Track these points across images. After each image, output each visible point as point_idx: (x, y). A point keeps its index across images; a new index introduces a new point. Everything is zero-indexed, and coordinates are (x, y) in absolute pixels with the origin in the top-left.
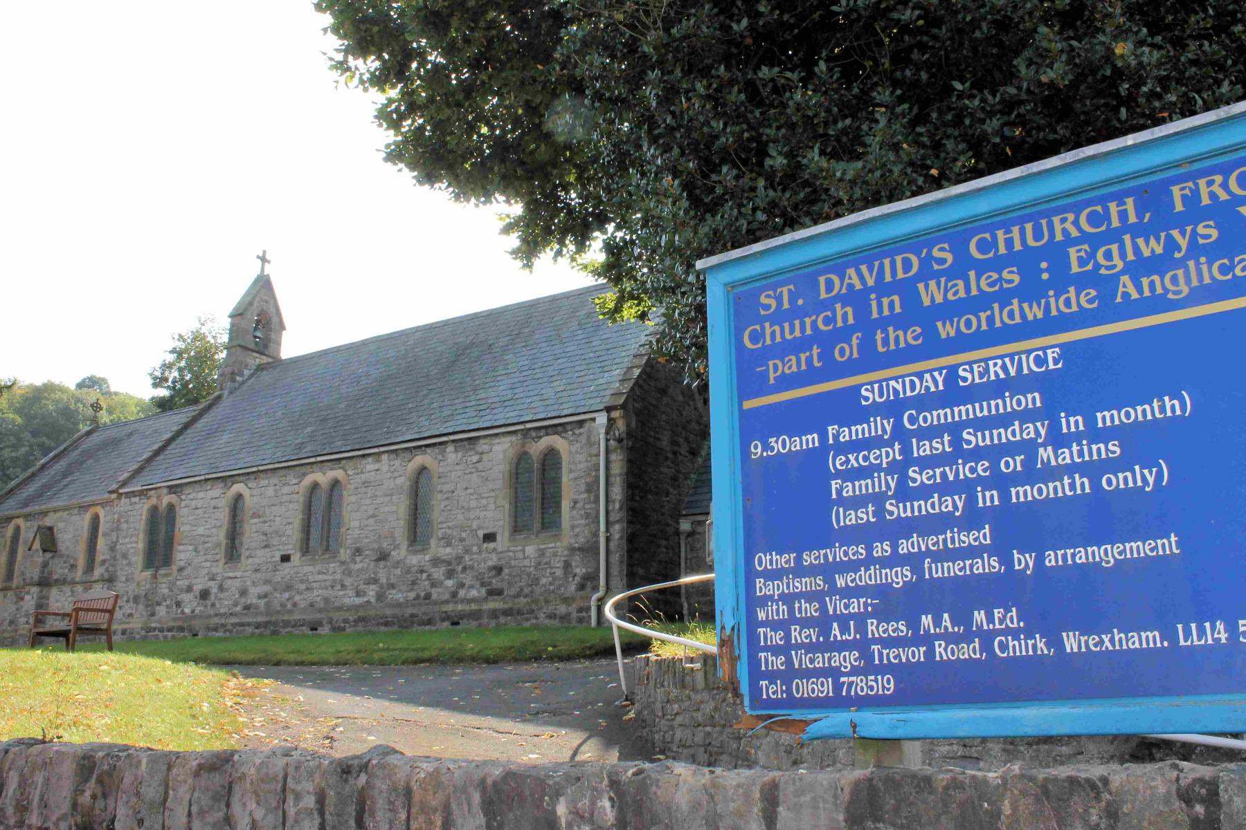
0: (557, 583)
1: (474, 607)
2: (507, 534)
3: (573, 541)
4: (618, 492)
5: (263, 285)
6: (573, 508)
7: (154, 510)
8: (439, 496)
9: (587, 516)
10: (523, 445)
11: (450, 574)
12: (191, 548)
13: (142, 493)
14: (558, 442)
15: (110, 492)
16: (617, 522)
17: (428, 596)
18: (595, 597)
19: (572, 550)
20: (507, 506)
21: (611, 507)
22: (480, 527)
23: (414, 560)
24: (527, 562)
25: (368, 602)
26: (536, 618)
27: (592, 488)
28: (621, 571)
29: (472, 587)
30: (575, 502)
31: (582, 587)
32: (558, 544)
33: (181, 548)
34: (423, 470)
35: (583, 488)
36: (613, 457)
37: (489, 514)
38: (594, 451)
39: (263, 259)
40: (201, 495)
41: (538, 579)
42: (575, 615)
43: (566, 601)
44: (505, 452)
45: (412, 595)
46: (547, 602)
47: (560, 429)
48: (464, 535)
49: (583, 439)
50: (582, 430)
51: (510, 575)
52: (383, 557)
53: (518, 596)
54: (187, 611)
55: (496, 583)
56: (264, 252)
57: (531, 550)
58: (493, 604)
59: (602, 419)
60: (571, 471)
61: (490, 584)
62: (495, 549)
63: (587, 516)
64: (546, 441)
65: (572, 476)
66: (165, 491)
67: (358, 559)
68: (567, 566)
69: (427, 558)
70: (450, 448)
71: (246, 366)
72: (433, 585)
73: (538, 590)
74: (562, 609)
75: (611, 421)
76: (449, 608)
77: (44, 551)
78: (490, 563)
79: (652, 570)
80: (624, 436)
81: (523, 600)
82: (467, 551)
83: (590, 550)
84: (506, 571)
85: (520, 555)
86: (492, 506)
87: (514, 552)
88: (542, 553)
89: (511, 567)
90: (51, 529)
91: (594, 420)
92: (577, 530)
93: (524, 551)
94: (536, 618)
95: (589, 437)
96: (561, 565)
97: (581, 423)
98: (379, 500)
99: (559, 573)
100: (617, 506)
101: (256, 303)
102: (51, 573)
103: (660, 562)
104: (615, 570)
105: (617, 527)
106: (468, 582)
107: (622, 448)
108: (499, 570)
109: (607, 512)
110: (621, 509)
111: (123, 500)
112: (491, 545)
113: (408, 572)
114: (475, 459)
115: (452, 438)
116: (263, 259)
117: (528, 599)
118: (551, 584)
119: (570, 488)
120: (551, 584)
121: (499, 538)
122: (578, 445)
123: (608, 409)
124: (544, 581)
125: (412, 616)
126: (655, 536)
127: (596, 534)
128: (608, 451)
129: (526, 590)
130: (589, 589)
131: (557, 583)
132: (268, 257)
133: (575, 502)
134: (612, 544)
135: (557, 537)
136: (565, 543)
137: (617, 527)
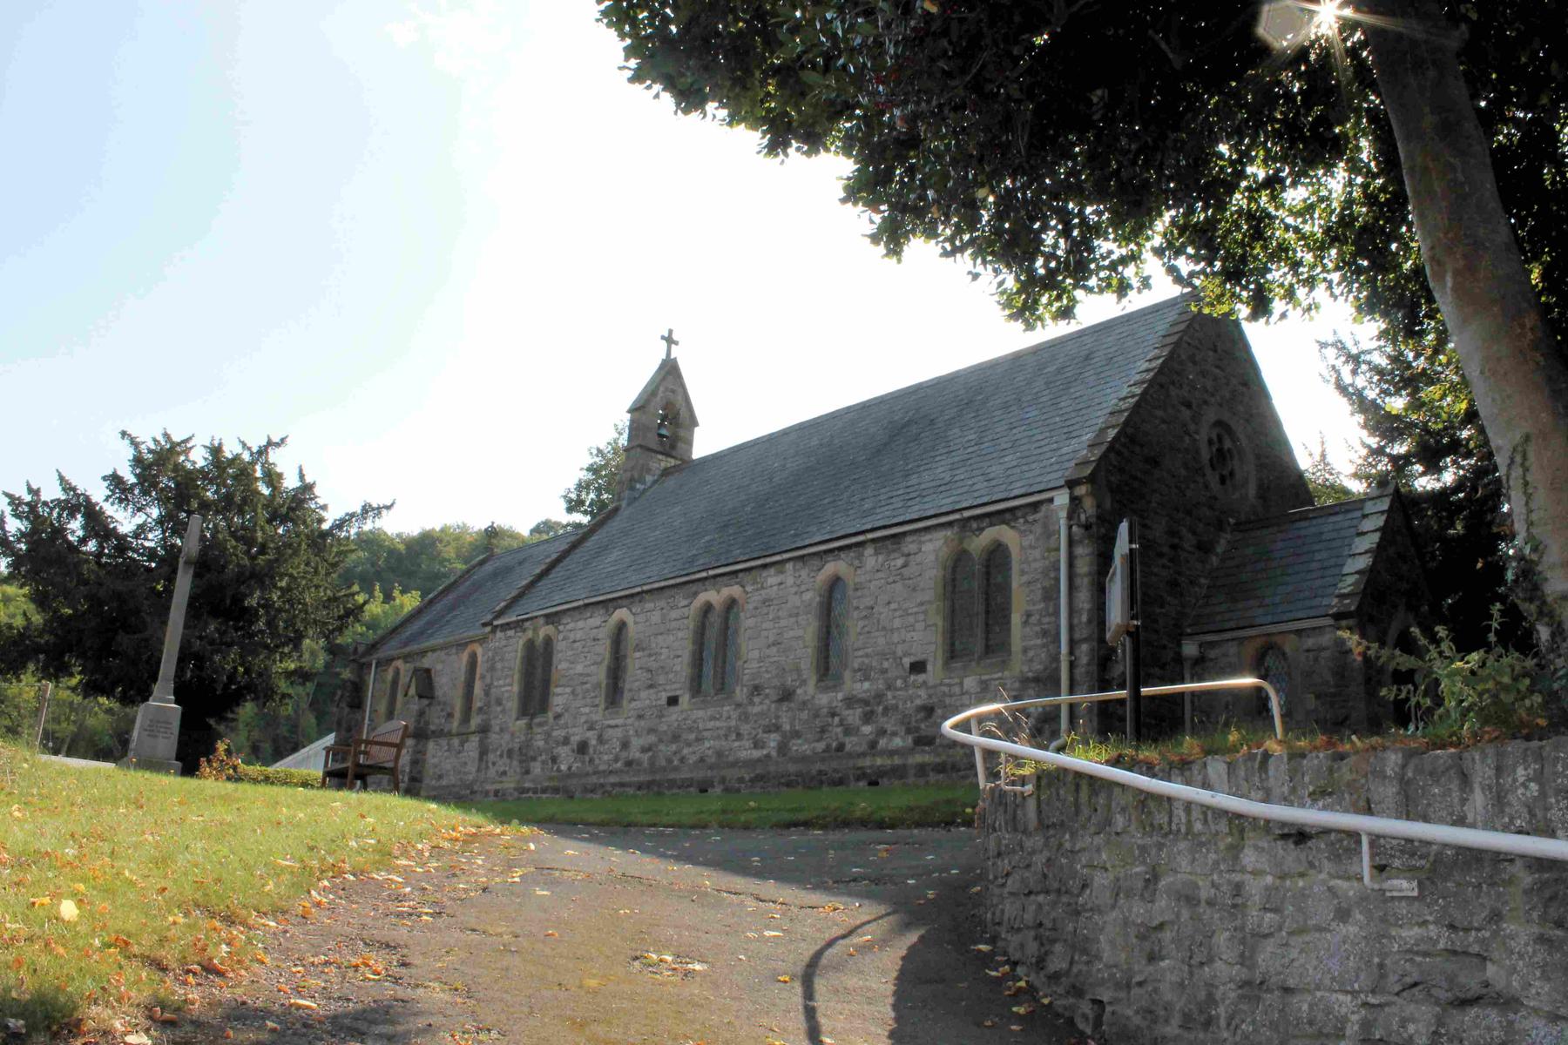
1: (897, 761)
2: (940, 662)
3: (1025, 669)
5: (669, 372)
6: (1026, 623)
7: (530, 645)
9: (1045, 633)
10: (961, 541)
11: (868, 717)
12: (568, 690)
13: (518, 625)
15: (484, 625)
17: (841, 747)
20: (940, 623)
21: (1076, 621)
23: (823, 699)
25: (768, 756)
27: (1050, 595)
29: (894, 734)
30: (1029, 615)
33: (559, 690)
35: (1039, 594)
39: (669, 340)
40: (581, 624)
45: (820, 746)
47: (1008, 516)
48: (886, 664)
49: (1038, 529)
50: (1037, 516)
52: (786, 696)
54: (563, 767)
56: (671, 332)
58: (918, 758)
59: (1062, 499)
60: (1023, 573)
61: (917, 729)
65: (1025, 579)
66: (542, 621)
67: (756, 700)
69: (840, 696)
71: (649, 471)
75: (1075, 501)
76: (867, 762)
78: (918, 702)
80: (1093, 520)
85: (957, 690)
87: (950, 685)
90: (428, 671)
91: (1051, 500)
92: (1031, 654)
93: (961, 684)
97: (1035, 506)
100: (1084, 618)
101: (660, 394)
105: (1085, 647)
106: (889, 728)
109: (1071, 628)
110: (1090, 621)
111: (499, 634)
112: (921, 678)
113: (816, 716)
114: (900, 562)
115: (870, 536)
116: (669, 340)
119: (1022, 599)
121: (929, 667)
122: (1031, 537)
123: (1071, 484)
127: (1056, 658)
128: (1071, 543)
132: (675, 337)
135: (1004, 664)
137: (1085, 647)
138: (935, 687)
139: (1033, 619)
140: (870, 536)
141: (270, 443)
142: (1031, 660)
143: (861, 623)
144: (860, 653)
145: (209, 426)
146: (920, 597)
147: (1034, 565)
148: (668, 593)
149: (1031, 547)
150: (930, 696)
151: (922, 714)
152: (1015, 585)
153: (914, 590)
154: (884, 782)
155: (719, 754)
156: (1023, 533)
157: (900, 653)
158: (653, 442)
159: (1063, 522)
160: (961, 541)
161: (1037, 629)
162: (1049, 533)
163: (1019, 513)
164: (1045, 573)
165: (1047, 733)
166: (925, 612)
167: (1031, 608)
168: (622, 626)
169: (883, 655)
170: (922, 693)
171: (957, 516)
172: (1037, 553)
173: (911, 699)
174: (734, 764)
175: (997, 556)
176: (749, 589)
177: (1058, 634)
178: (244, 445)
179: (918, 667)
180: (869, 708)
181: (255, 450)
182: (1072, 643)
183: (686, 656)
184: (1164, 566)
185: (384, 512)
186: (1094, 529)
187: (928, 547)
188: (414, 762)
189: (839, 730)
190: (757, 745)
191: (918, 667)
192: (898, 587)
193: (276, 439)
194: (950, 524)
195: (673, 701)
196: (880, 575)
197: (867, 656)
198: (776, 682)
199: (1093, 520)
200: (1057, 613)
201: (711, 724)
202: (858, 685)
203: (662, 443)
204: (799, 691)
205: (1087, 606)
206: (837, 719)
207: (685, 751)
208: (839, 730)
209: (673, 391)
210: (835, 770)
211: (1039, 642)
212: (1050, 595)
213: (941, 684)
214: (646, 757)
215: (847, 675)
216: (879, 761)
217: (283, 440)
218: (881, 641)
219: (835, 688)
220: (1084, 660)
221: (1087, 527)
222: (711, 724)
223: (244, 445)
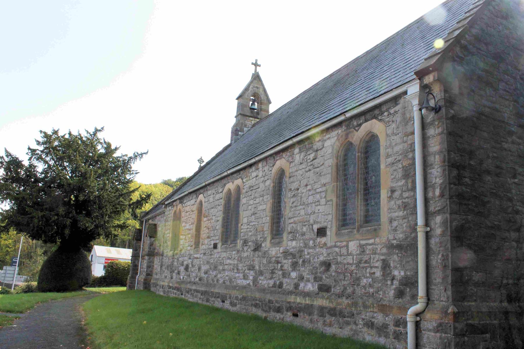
0: (376, 285)
1: (308, 301)
2: (334, 228)
3: (391, 237)
4: (437, 175)
5: (256, 77)
6: (390, 198)
8: (290, 194)
9: (405, 206)
10: (347, 135)
11: (295, 265)
14: (375, 126)
16: (439, 212)
17: (281, 285)
18: (413, 310)
19: (391, 247)
20: (334, 200)
21: (430, 195)
22: (315, 222)
23: (274, 251)
24: (349, 259)
25: (249, 284)
26: (355, 323)
27: (408, 174)
28: (444, 278)
29: (308, 281)
30: (393, 191)
31: (400, 294)
32: (377, 240)
34: (282, 173)
35: (400, 174)
36: (431, 132)
37: (321, 208)
38: (409, 130)
39: (256, 65)
41: (358, 279)
42: (392, 328)
43: (384, 309)
44: (332, 146)
45: (271, 282)
46: (365, 307)
47: (377, 112)
48: (305, 229)
49: (398, 118)
50: (397, 108)
51: (336, 271)
52: (257, 248)
53: (340, 296)
54: (182, 277)
55: (326, 280)
56: (256, 60)
57: (353, 246)
58: (320, 302)
59: (414, 89)
60: (388, 156)
61: (321, 279)
62: (325, 244)
63: (405, 206)
64: (366, 127)
65: (390, 160)
66: (178, 201)
67: (245, 248)
68: (385, 266)
69: (281, 250)
70: (297, 150)
71: (246, 126)
72: (284, 275)
73: (359, 291)
74: (379, 318)
75: (425, 89)
76: (291, 299)
77: (150, 237)
78: (322, 258)
79: (497, 273)
80: (442, 103)
81: (345, 301)
82: (306, 246)
83: (407, 248)
84: (333, 267)
85: (344, 251)
86: (323, 201)
87: (341, 247)
88: (362, 248)
89: (337, 263)
90: (155, 225)
91: (405, 93)
92: (395, 224)
93: (347, 246)
94: (355, 323)
95: (404, 114)
96: (379, 264)
97: (395, 100)
98: (258, 200)
99: (378, 273)
100: (437, 192)
101: (250, 89)
102: (155, 249)
103: (509, 260)
104: (438, 276)
105: (438, 219)
106: (306, 275)
107: (439, 119)
108: (327, 265)
109: (426, 201)
110: (442, 195)
112: (323, 240)
113: (270, 262)
114: (312, 156)
115: (295, 140)
116: (256, 65)
117: (349, 301)
118: (371, 286)
119: (388, 177)
120: (371, 286)
121: (328, 233)
122: (394, 125)
123: (421, 74)
124: (364, 281)
125: (270, 301)
126: (499, 228)
127: (414, 229)
128: (424, 126)
129: (349, 290)
130: (407, 298)
131: (376, 285)
132: (259, 63)
133: (393, 191)
134: (433, 241)
135: (376, 232)
136: (384, 240)
137: (438, 219)
138: (330, 247)
139: (397, 194)
140: (295, 140)
141: (97, 131)
142: (395, 230)
143: (292, 200)
144: (292, 220)
145: (73, 124)
146: (323, 180)
147: (396, 149)
148: (216, 184)
149: (394, 134)
150: (328, 254)
151: (323, 268)
152: (382, 166)
153: (320, 175)
154: (301, 314)
155: (230, 280)
156: (387, 124)
157: (311, 222)
158: (248, 112)
159: (416, 108)
160: (347, 135)
161: (399, 202)
162: (407, 121)
163: (384, 108)
164: (405, 154)
165: (407, 298)
166: (326, 191)
167: (394, 185)
168: (201, 203)
169: (304, 223)
170: (324, 251)
171: (342, 118)
172: (397, 139)
173: (318, 255)
174: (234, 288)
175: (371, 143)
176: (244, 180)
177: (415, 206)
178: (88, 132)
179: (322, 232)
180: (296, 258)
181: (92, 133)
182: (427, 215)
183: (268, 213)
184: (513, 143)
185: (144, 155)
186: (443, 110)
187: (328, 143)
188: (149, 267)
189: (280, 273)
190: (245, 277)
191: (322, 232)
192: (311, 174)
193: (99, 128)
194: (339, 124)
195: (215, 246)
196: (303, 166)
197: (295, 223)
198: (254, 238)
199: (442, 103)
200: (414, 189)
201: (228, 261)
202: (290, 243)
203: (252, 112)
204: (263, 245)
205: (439, 181)
206: (279, 265)
207: (219, 276)
208: (280, 273)
209: (257, 88)
210: (277, 302)
211: (401, 213)
212: (408, 174)
213: (335, 246)
214: (206, 276)
215: (285, 235)
216: (298, 300)
217: (102, 128)
218: (302, 212)
219: (279, 244)
220: (439, 231)
221: (436, 110)
222: (228, 261)
223: (88, 132)
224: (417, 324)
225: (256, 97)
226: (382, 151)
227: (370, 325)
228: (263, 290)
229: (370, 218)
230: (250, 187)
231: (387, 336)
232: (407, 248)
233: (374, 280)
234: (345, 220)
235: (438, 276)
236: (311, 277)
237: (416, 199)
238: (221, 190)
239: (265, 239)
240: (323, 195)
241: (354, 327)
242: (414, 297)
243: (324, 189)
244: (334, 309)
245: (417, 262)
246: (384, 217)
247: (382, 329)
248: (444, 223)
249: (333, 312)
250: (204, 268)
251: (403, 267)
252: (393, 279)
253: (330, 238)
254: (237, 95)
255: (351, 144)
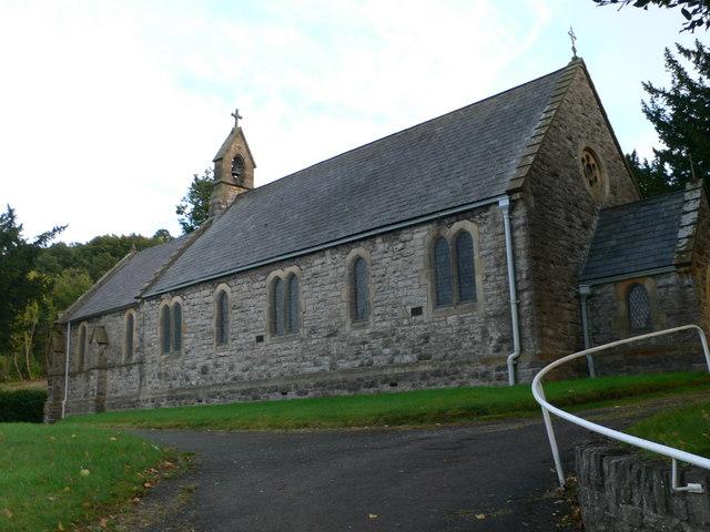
4: (523, 263)
5: (237, 134)
10: (439, 230)
17: (370, 364)
19: (487, 317)
24: (449, 330)
27: (500, 263)
38: (500, 231)
39: (236, 116)
43: (486, 362)
50: (488, 213)
64: (457, 226)
68: (485, 333)
76: (388, 372)
84: (433, 338)
90: (103, 327)
91: (497, 203)
96: (479, 330)
97: (486, 207)
100: (524, 276)
105: (525, 294)
108: (426, 338)
109: (516, 282)
112: (419, 318)
115: (380, 231)
116: (236, 116)
119: (481, 266)
129: (451, 353)
132: (240, 114)
135: (474, 308)
140: (380, 231)
146: (415, 268)
152: (476, 257)
156: (479, 225)
160: (439, 230)
162: (497, 223)
180: (387, 337)
182: (518, 293)
188: (100, 384)
191: (417, 311)
195: (260, 339)
205: (525, 269)
210: (368, 378)
212: (500, 263)
216: (396, 371)
224: (515, 366)
225: (238, 161)
226: (475, 245)
227: (475, 376)
228: (344, 372)
229: (466, 293)
230: (314, 274)
231: (490, 381)
232: (504, 315)
233: (475, 343)
234: (438, 300)
235: (527, 332)
236: (409, 350)
237: (508, 283)
238: (262, 278)
239: (343, 325)
240: (417, 280)
241: (460, 380)
242: (511, 349)
243: (417, 275)
244: (438, 371)
245: (511, 325)
246: (480, 295)
247: (485, 376)
248: (531, 297)
249: (437, 374)
250: (239, 366)
251: (499, 330)
252: (492, 339)
253: (427, 314)
254: (213, 157)
255: (442, 237)
